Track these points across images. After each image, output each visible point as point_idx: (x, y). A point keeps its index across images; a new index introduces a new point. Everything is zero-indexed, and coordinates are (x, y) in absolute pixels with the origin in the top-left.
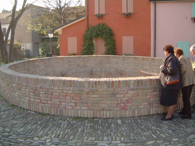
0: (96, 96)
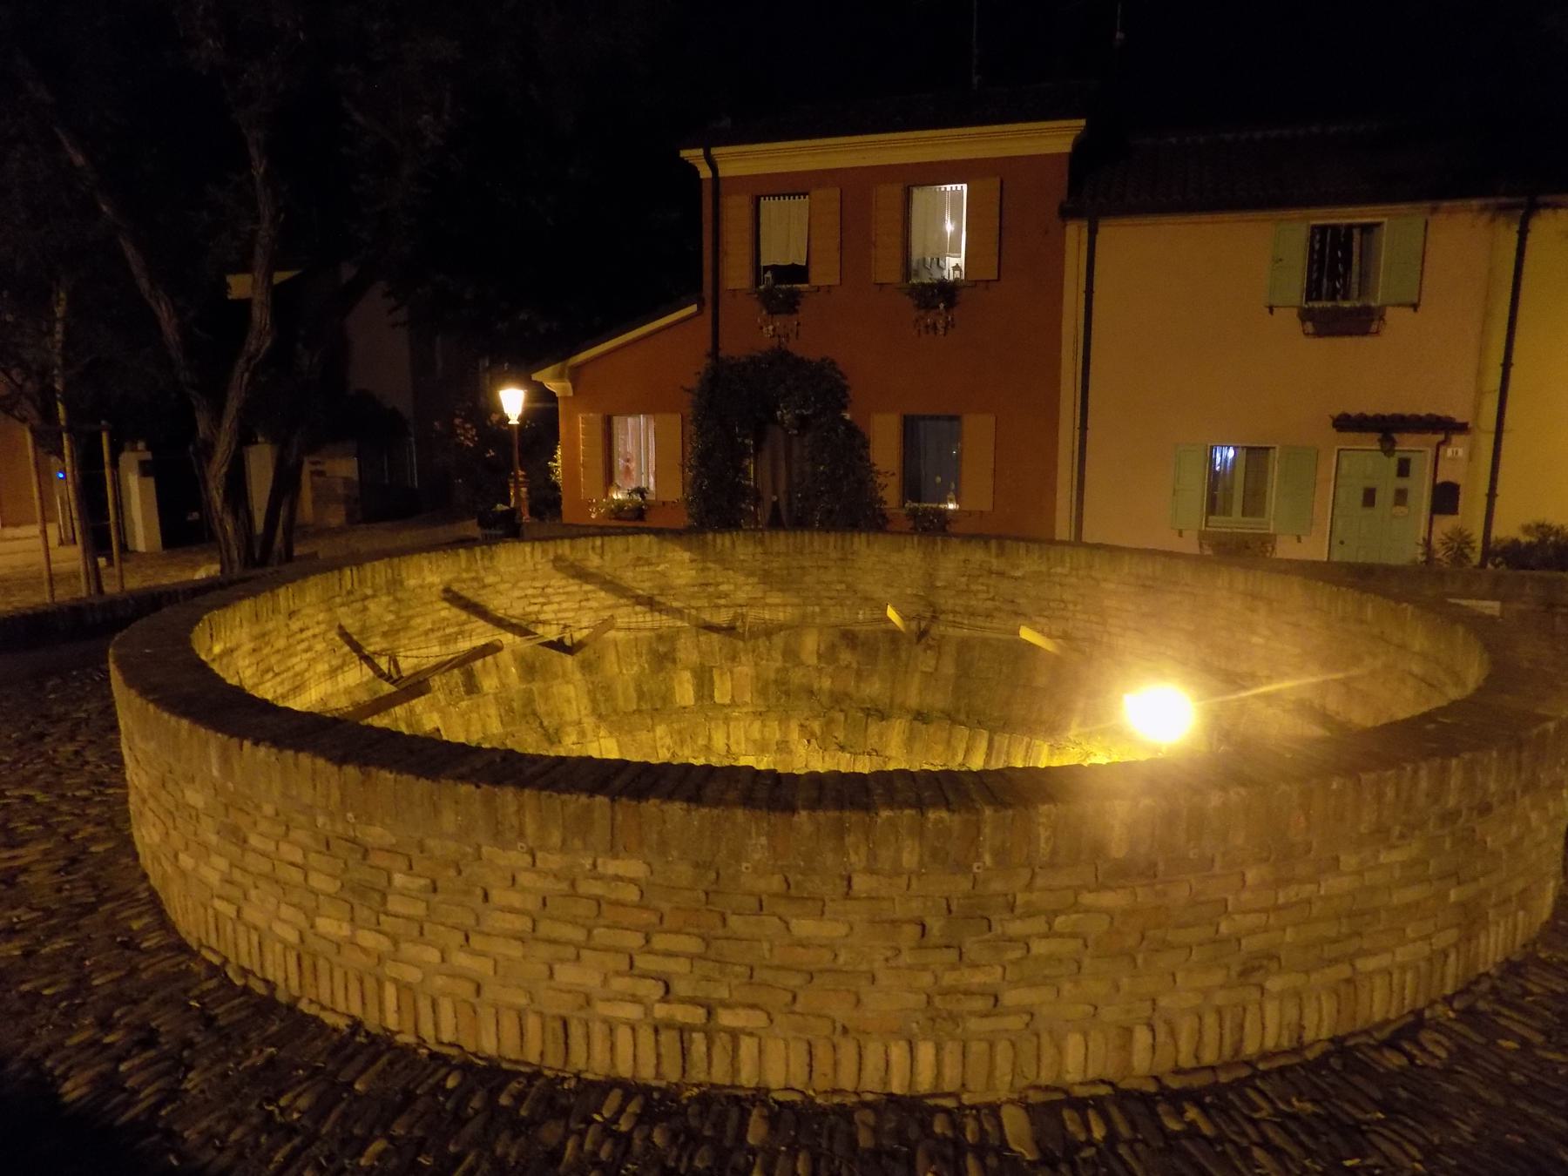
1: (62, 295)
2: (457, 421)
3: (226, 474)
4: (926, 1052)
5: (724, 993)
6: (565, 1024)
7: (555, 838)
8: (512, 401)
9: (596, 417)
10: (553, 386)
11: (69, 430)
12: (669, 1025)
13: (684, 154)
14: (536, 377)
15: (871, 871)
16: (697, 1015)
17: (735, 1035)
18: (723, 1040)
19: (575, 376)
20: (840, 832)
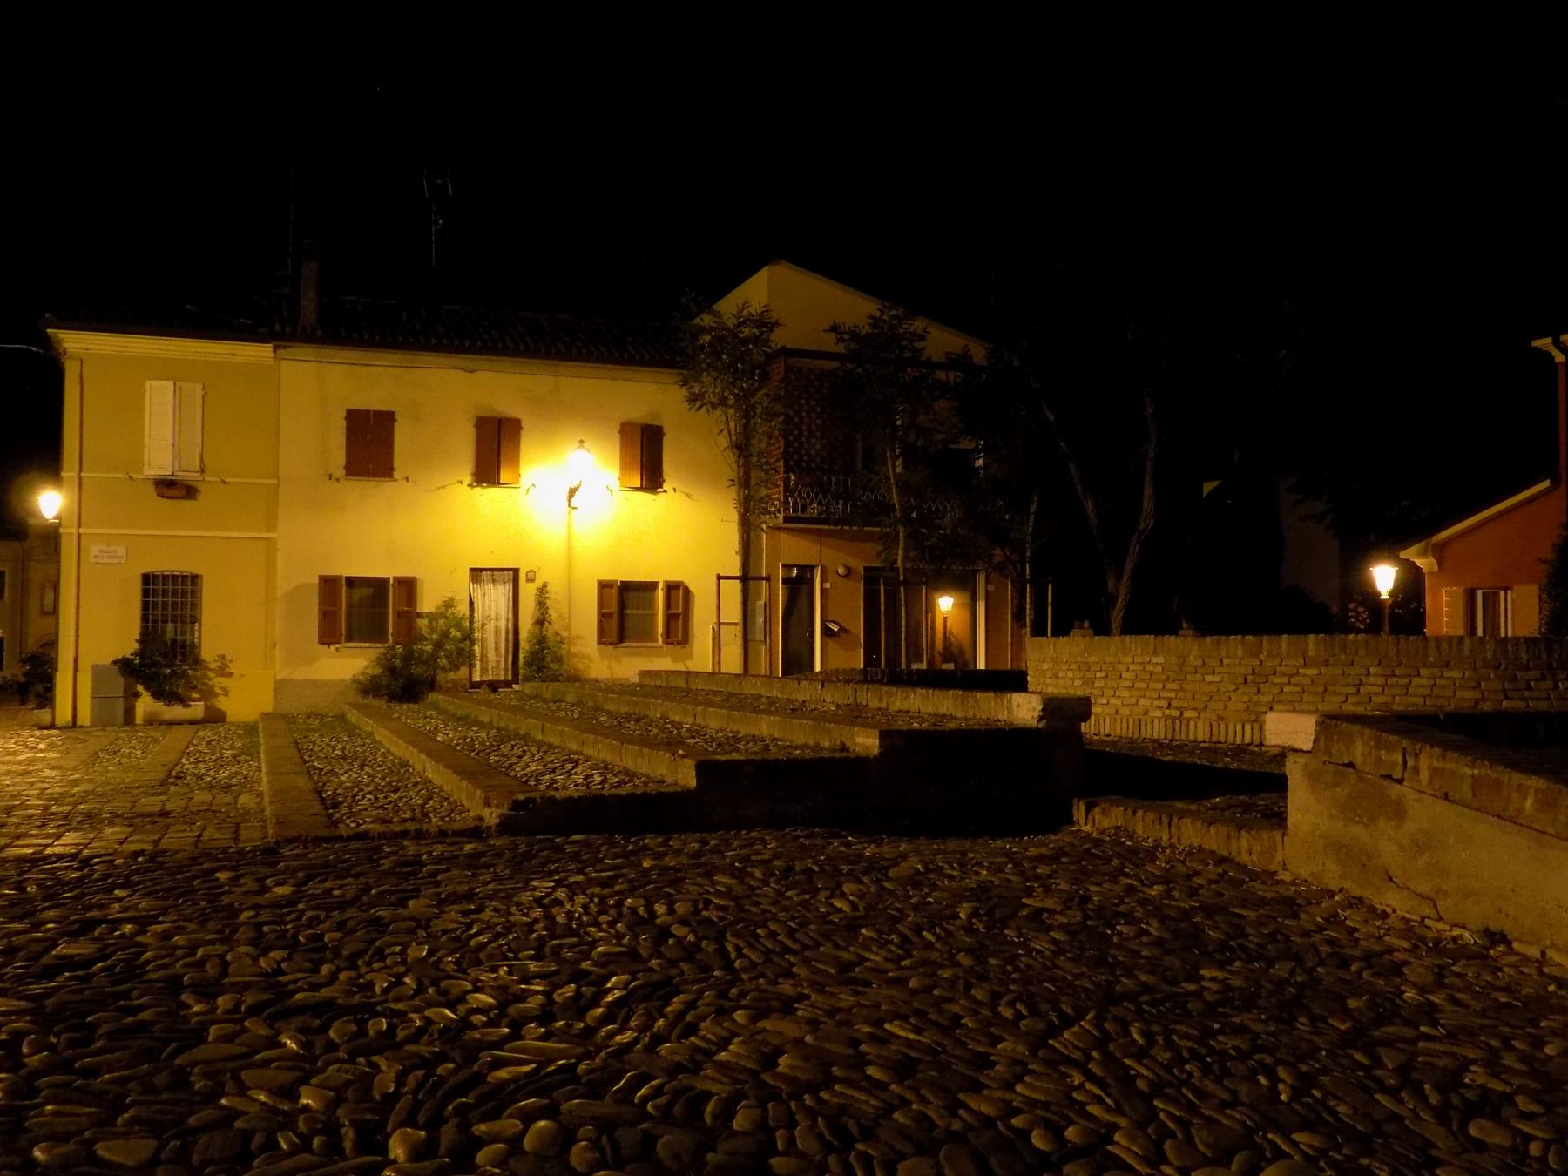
0: (1217, 678)
1: (1036, 499)
2: (1352, 606)
3: (1123, 618)
4: (1248, 728)
5: (1186, 705)
6: (1140, 720)
7: (1139, 651)
8: (1384, 577)
9: (1458, 591)
10: (1419, 562)
11: (1030, 581)
12: (1169, 716)
13: (1537, 343)
14: (1404, 554)
15: (1228, 657)
16: (1177, 713)
17: (1189, 720)
18: (1184, 722)
19: (1439, 552)
20: (1219, 643)
